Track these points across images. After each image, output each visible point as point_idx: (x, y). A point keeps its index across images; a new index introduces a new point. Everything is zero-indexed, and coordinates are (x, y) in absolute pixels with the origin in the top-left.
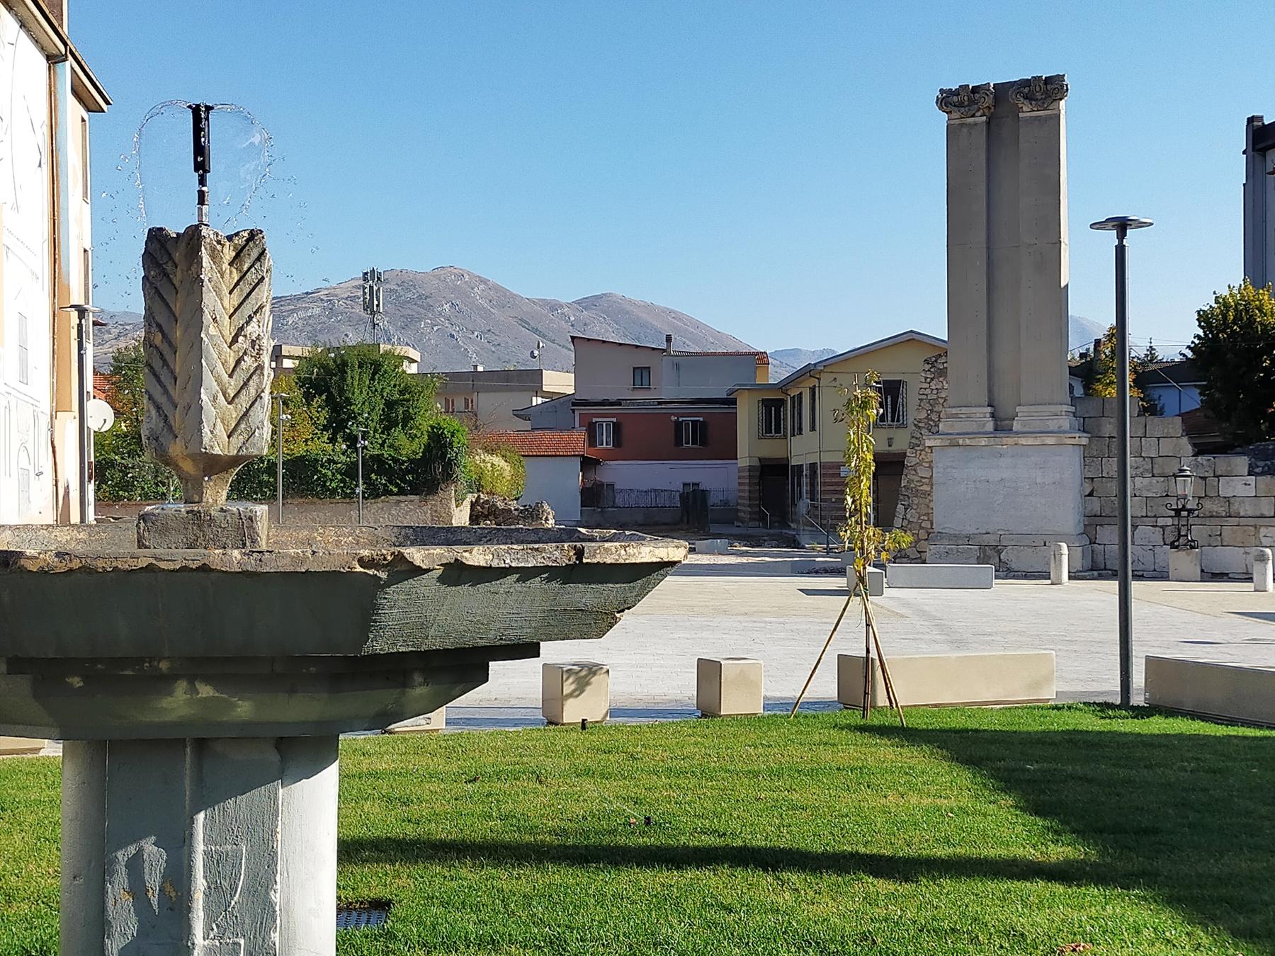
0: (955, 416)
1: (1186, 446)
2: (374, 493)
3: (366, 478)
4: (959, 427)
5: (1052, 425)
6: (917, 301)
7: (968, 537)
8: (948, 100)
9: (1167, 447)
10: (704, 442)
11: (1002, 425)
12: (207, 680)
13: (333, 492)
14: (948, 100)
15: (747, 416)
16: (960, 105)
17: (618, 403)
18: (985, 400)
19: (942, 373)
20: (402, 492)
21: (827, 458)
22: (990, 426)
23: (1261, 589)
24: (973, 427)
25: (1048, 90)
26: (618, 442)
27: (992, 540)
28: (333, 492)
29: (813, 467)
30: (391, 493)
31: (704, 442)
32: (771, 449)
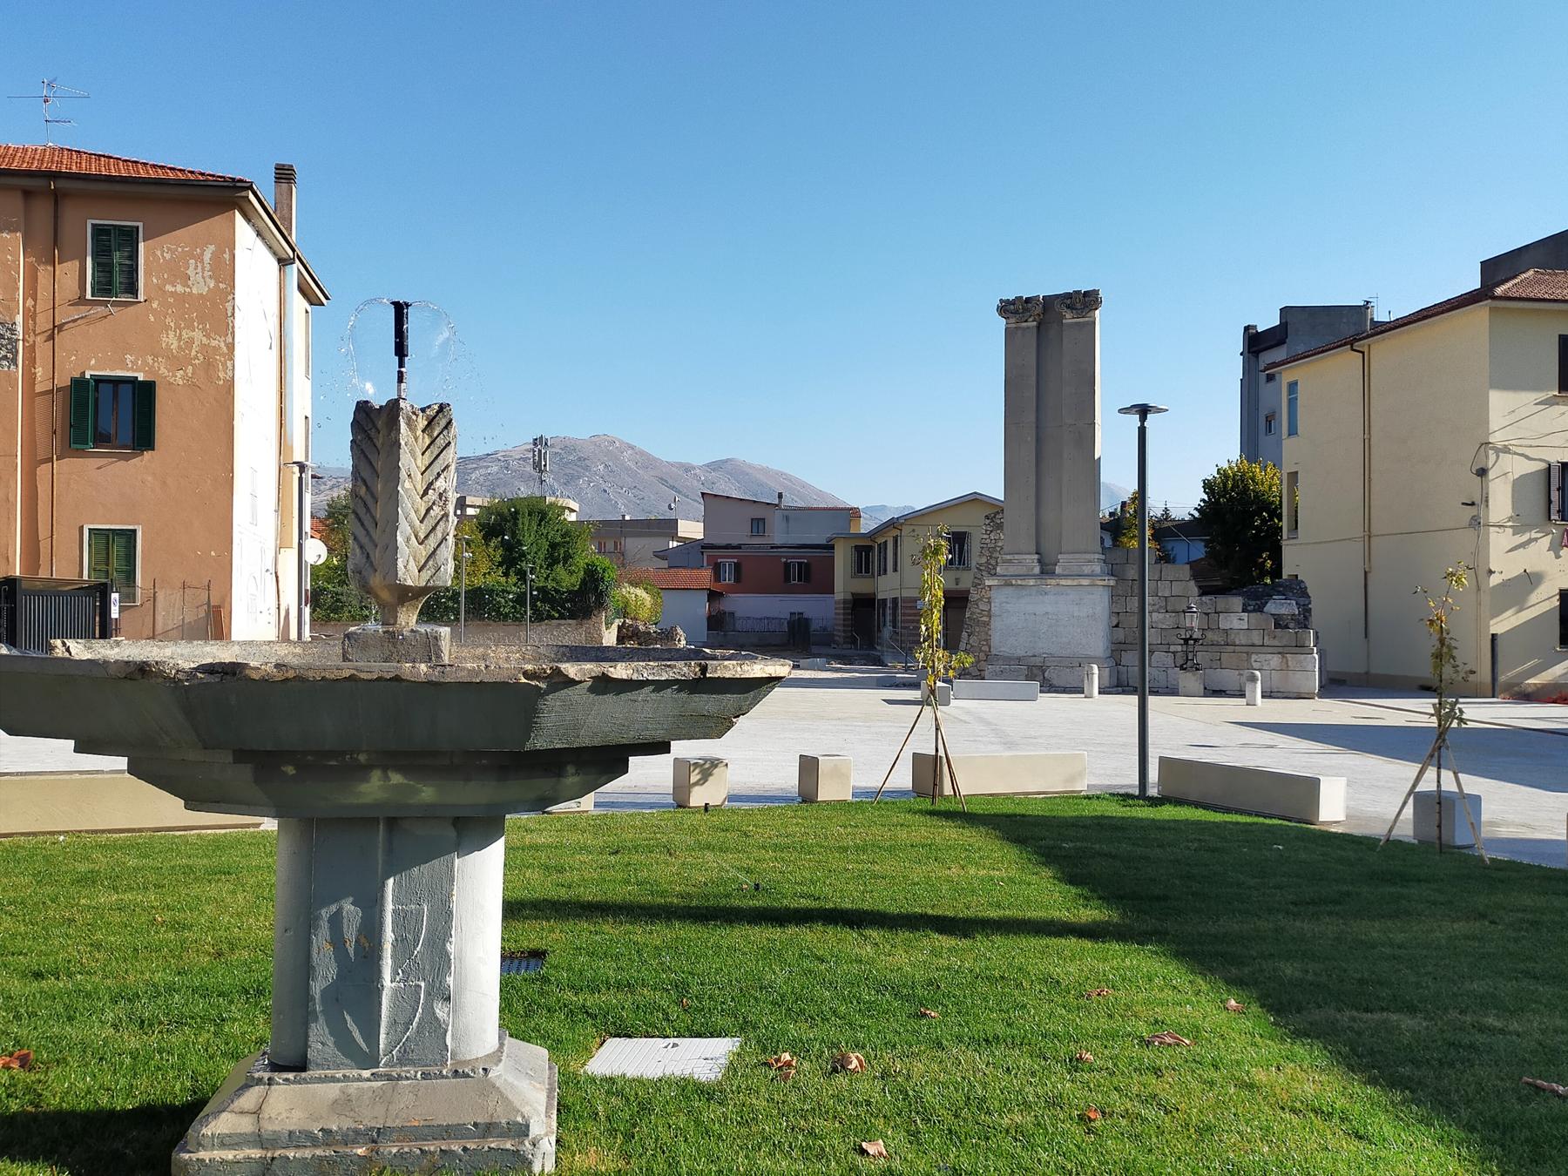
0: (1010, 561)
1: (1193, 588)
2: (539, 617)
3: (533, 606)
4: (1012, 570)
5: (1087, 570)
6: (982, 471)
7: (1019, 659)
8: (1007, 308)
9: (1177, 589)
10: (808, 579)
11: (1047, 570)
12: (400, 769)
13: (506, 616)
14: (1007, 308)
15: (842, 560)
16: (1016, 312)
17: (739, 547)
18: (1033, 549)
19: (1000, 527)
20: (562, 617)
21: (906, 594)
22: (1037, 570)
23: (1251, 704)
24: (1023, 571)
25: (1086, 301)
26: (738, 579)
27: (1038, 661)
28: (506, 616)
29: (895, 600)
30: (551, 617)
31: (808, 579)
32: (862, 586)
